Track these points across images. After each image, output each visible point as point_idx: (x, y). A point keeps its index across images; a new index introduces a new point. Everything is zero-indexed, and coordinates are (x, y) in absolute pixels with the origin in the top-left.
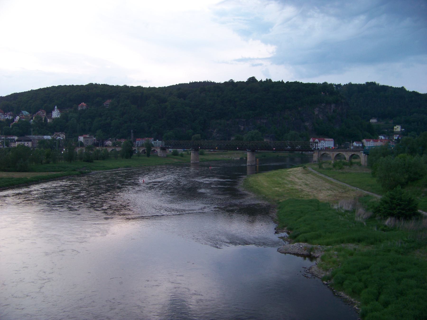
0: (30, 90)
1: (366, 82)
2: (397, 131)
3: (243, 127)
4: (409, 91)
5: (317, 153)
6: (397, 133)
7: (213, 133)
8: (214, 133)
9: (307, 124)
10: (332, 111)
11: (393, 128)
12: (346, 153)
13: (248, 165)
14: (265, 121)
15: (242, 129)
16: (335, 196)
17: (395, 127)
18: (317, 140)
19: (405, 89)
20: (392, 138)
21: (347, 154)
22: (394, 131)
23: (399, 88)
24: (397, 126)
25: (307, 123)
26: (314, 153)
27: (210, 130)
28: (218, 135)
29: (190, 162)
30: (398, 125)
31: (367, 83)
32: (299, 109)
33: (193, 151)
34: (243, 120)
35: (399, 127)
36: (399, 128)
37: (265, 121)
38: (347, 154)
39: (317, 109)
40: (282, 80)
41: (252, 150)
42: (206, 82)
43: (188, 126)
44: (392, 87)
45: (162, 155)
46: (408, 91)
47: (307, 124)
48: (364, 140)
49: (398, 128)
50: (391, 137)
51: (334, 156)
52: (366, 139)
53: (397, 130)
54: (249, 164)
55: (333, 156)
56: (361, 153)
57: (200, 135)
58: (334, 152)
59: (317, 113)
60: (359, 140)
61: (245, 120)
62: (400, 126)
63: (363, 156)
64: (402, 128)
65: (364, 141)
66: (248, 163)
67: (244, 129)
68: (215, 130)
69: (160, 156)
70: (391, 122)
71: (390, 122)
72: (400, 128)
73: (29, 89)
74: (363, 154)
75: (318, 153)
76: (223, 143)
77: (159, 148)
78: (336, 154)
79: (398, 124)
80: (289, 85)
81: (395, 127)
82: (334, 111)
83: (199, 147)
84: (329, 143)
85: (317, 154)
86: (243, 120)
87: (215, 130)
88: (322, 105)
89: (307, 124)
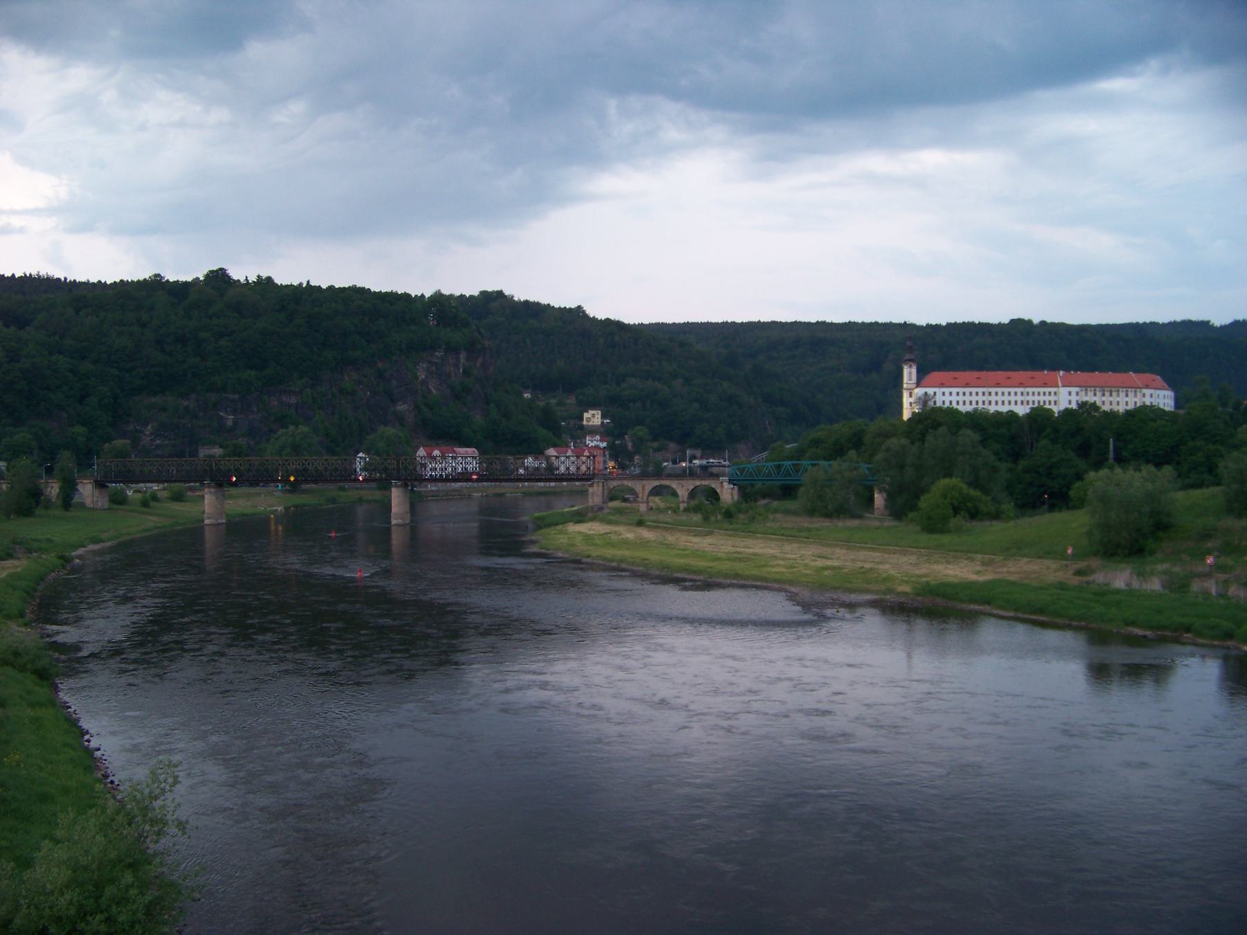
0: (794, 320)
1: (482, 290)
2: (593, 426)
3: (232, 417)
4: (596, 317)
5: (601, 484)
6: (593, 431)
7: (141, 435)
8: (145, 435)
9: (401, 407)
10: (461, 371)
11: (581, 419)
12: (679, 484)
13: (397, 525)
14: (293, 400)
15: (230, 423)
16: (164, 607)
17: (586, 415)
18: (436, 453)
19: (584, 312)
20: (581, 442)
21: (683, 486)
22: (583, 425)
23: (570, 309)
24: (591, 412)
25: (401, 405)
26: (592, 485)
27: (131, 427)
28: (158, 442)
29: (203, 521)
30: (592, 410)
31: (484, 294)
32: (380, 365)
33: (212, 490)
34: (231, 396)
35: (598, 414)
36: (596, 416)
37: (293, 400)
38: (683, 486)
39: (424, 365)
40: (308, 282)
41: (216, 484)
42: (304, 286)
43: (65, 415)
44: (549, 305)
45: (100, 504)
46: (594, 317)
47: (403, 407)
48: (552, 449)
49: (593, 418)
50: (578, 441)
51: (647, 492)
52: (556, 449)
53: (591, 423)
54: (400, 521)
55: (643, 493)
56: (722, 482)
57: (129, 442)
58: (645, 482)
59: (423, 377)
60: (538, 452)
61: (237, 396)
62: (600, 412)
63: (729, 491)
64: (603, 417)
65: (551, 452)
66: (397, 519)
67: (235, 423)
68: (149, 427)
69: (92, 506)
70: (571, 400)
71: (569, 401)
72: (600, 416)
73: (704, 320)
74: (726, 485)
75: (603, 486)
76: (313, 464)
77: (90, 483)
78: (651, 487)
79: (593, 406)
80: (123, 289)
81: (586, 415)
82: (466, 373)
83: (232, 477)
84: (466, 459)
85: (601, 488)
86: (231, 396)
87: (148, 425)
88: (437, 353)
89: (401, 407)
